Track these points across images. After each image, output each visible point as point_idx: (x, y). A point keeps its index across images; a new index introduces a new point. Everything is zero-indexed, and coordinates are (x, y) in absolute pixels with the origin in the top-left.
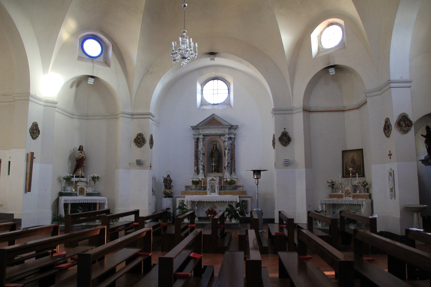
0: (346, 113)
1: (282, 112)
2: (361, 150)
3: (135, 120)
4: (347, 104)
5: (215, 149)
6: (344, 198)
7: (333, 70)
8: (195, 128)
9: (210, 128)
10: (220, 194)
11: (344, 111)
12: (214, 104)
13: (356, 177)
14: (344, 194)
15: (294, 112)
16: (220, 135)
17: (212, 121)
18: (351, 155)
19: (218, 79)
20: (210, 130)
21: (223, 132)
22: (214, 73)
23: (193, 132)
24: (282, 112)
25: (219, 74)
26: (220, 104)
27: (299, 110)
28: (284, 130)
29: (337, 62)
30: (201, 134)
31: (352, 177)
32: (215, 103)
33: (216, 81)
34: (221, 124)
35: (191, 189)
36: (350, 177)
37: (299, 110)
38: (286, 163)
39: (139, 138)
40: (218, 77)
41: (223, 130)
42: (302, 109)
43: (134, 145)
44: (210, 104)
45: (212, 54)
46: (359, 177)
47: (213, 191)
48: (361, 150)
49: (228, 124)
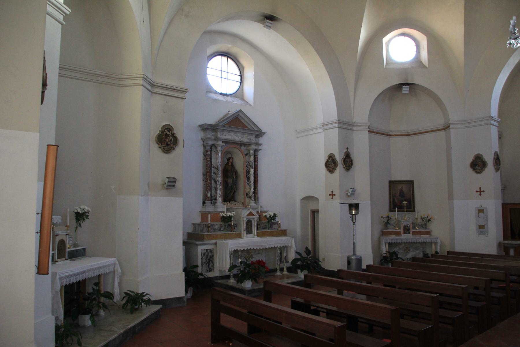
0: (392, 138)
1: (345, 126)
2: (411, 183)
3: (158, 97)
4: (393, 128)
5: (230, 164)
6: (403, 235)
7: (403, 88)
8: (204, 128)
9: (233, 131)
10: (258, 235)
11: (391, 135)
12: (221, 94)
13: (395, 211)
14: (402, 231)
15: (355, 128)
16: (241, 144)
17: (237, 121)
18: (399, 187)
19: (228, 57)
20: (232, 134)
21: (248, 141)
22: (229, 46)
23: (201, 135)
24: (345, 126)
25: (235, 50)
26: (230, 95)
27: (364, 127)
28: (346, 150)
29: (417, 81)
30: (220, 139)
31: (406, 211)
32: (223, 92)
33: (225, 59)
34: (247, 127)
35: (214, 230)
36: (404, 211)
37: (364, 127)
38: (170, 184)
39: (166, 135)
40: (229, 54)
41: (249, 137)
42: (337, 125)
43: (155, 148)
44: (216, 93)
45: (270, 19)
46: (398, 211)
47: (249, 231)
48: (411, 183)
49: (256, 129)
